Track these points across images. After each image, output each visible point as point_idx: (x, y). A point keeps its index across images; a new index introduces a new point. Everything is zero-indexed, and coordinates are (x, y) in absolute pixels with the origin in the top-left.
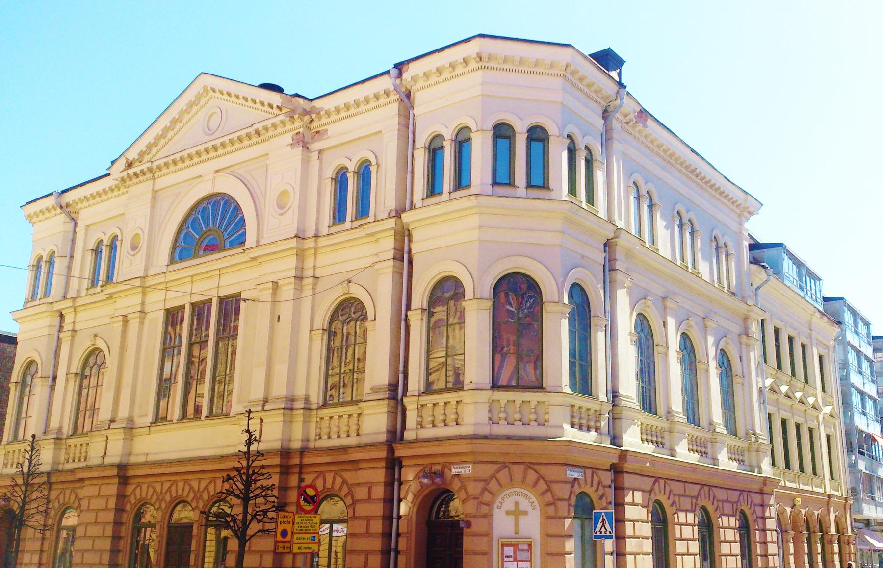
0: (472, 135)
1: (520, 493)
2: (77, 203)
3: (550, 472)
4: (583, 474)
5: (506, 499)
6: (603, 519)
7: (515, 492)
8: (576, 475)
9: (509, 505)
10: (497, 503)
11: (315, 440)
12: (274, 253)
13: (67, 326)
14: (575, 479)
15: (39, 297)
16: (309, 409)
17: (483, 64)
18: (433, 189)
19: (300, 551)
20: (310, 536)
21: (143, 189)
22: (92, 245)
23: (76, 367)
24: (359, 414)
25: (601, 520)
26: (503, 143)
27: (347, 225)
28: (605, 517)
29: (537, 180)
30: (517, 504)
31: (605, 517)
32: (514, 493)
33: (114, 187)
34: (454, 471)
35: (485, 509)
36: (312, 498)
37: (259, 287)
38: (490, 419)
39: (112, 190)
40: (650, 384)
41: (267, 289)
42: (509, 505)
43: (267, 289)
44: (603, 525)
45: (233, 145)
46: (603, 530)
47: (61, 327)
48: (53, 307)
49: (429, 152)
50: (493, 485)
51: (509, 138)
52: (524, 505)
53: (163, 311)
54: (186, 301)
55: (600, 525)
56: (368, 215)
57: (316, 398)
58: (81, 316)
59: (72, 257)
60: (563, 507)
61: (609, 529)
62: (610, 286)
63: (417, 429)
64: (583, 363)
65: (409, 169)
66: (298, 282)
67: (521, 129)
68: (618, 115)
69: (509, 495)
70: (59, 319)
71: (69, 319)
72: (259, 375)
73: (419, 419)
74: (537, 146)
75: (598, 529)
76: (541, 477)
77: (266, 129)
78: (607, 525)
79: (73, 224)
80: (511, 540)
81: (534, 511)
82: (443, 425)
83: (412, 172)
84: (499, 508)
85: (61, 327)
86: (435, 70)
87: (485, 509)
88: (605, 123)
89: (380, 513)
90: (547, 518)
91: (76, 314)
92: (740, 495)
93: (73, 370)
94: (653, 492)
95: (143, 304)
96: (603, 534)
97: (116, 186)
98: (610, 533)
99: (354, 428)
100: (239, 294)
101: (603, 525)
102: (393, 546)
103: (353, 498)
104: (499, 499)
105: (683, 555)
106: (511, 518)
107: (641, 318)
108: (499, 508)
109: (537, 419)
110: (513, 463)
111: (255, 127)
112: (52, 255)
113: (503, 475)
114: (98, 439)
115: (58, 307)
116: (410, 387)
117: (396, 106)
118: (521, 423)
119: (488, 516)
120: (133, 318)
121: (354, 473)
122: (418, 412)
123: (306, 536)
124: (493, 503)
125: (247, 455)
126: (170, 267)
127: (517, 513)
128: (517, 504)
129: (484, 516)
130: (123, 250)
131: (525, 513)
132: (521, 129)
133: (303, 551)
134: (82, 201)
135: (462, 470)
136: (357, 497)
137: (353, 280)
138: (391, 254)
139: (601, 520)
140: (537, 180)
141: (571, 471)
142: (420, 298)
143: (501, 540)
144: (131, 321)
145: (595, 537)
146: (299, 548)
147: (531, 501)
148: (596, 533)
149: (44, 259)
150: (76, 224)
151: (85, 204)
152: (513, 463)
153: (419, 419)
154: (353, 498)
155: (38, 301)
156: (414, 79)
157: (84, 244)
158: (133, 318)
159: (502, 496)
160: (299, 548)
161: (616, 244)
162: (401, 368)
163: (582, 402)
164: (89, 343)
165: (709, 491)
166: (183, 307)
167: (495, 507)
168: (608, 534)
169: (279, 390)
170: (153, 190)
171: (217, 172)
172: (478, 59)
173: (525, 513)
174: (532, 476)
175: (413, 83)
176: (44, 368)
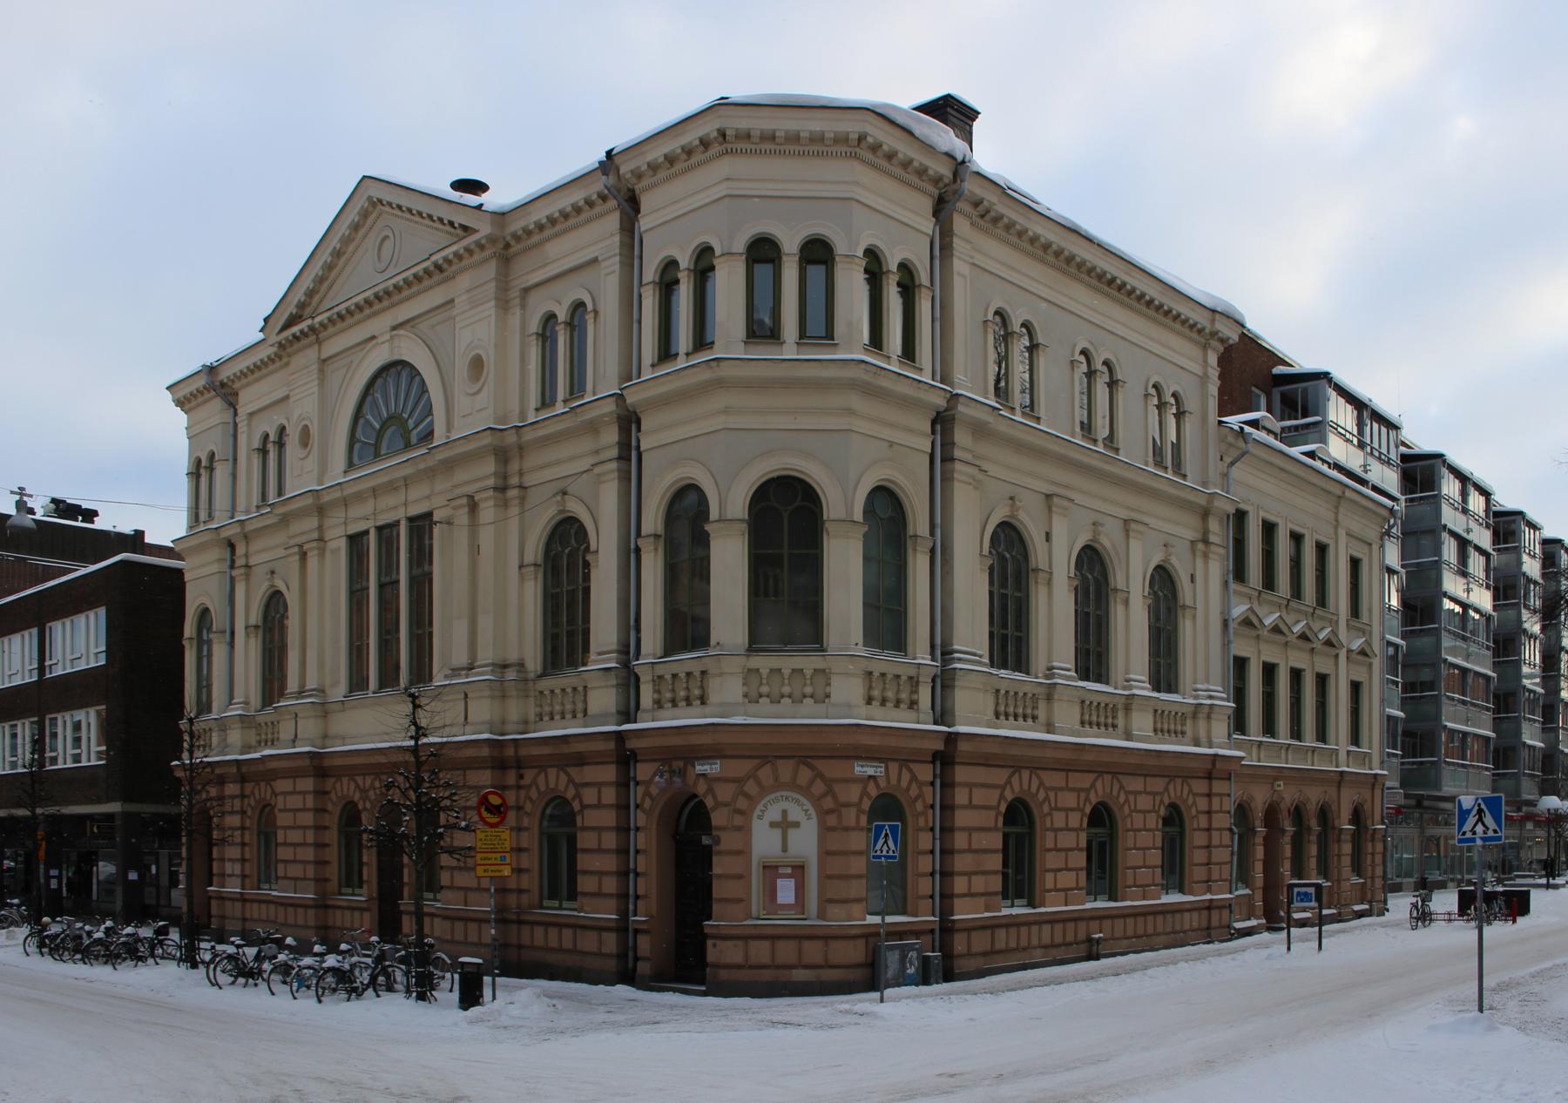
0: (716, 262)
2: (233, 381)
3: (832, 769)
4: (883, 769)
5: (769, 807)
6: (886, 835)
8: (870, 771)
9: (774, 813)
10: (757, 812)
11: (536, 722)
13: (240, 562)
14: (870, 777)
15: (561, 395)
16: (526, 680)
17: (729, 147)
18: (666, 353)
19: (486, 874)
20: (498, 855)
21: (307, 358)
22: (256, 444)
23: (255, 617)
24: (585, 687)
25: (883, 835)
26: (763, 271)
27: (560, 408)
28: (1483, 806)
29: (816, 325)
30: (785, 813)
31: (1483, 806)
33: (273, 356)
34: (699, 769)
35: (738, 820)
36: (497, 808)
37: (454, 504)
38: (745, 696)
39: (273, 361)
41: (461, 506)
43: (461, 506)
44: (886, 842)
45: (400, 292)
46: (1479, 829)
47: (233, 561)
48: (219, 534)
49: (660, 290)
50: (751, 787)
51: (771, 261)
52: (795, 813)
53: (344, 538)
54: (400, 514)
55: (881, 841)
56: (583, 389)
57: (534, 663)
58: (256, 545)
59: (235, 460)
60: (850, 817)
61: (892, 847)
63: (653, 709)
65: (635, 317)
66: (499, 495)
67: (790, 245)
68: (961, 205)
69: (776, 800)
70: (229, 549)
71: (240, 550)
72: (460, 630)
73: (656, 696)
74: (816, 273)
75: (1467, 827)
76: (820, 776)
77: (448, 261)
78: (891, 842)
79: (232, 410)
82: (699, 702)
83: (640, 322)
84: (760, 817)
85: (233, 561)
86: (697, 142)
87: (738, 820)
89: (613, 824)
90: (825, 830)
91: (247, 543)
93: (529, 558)
95: (320, 528)
96: (884, 853)
97: (276, 354)
98: (1495, 831)
99: (580, 706)
100: (429, 515)
101: (886, 842)
102: (632, 866)
103: (581, 802)
104: (760, 807)
106: (777, 833)
108: (760, 817)
110: (777, 757)
111: (434, 258)
112: (212, 455)
113: (765, 773)
114: (287, 717)
115: (225, 534)
116: (644, 650)
117: (616, 216)
118: (790, 701)
119: (745, 830)
120: (311, 549)
121: (578, 769)
122: (654, 685)
123: (494, 855)
124: (752, 811)
125: (415, 750)
126: (541, 412)
127: (785, 825)
128: (785, 813)
129: (739, 829)
130: (292, 449)
131: (797, 825)
132: (790, 245)
133: (490, 874)
134: (239, 378)
135: (707, 767)
136: (586, 802)
137: (569, 490)
138: (614, 452)
139: (883, 835)
140: (816, 325)
141: (862, 766)
142: (653, 520)
144: (482, 505)
145: (874, 857)
146: (485, 871)
147: (805, 808)
148: (1464, 833)
149: (272, 438)
150: (236, 414)
151: (244, 381)
152: (777, 757)
153: (656, 696)
154: (581, 802)
155: (682, 357)
157: (248, 441)
158: (311, 549)
159: (763, 802)
160: (485, 871)
161: (954, 419)
162: (632, 622)
163: (887, 662)
164: (266, 585)
167: (755, 816)
168: (891, 853)
169: (486, 655)
170: (319, 358)
171: (394, 328)
172: (721, 139)
173: (797, 825)
174: (805, 774)
176: (219, 619)
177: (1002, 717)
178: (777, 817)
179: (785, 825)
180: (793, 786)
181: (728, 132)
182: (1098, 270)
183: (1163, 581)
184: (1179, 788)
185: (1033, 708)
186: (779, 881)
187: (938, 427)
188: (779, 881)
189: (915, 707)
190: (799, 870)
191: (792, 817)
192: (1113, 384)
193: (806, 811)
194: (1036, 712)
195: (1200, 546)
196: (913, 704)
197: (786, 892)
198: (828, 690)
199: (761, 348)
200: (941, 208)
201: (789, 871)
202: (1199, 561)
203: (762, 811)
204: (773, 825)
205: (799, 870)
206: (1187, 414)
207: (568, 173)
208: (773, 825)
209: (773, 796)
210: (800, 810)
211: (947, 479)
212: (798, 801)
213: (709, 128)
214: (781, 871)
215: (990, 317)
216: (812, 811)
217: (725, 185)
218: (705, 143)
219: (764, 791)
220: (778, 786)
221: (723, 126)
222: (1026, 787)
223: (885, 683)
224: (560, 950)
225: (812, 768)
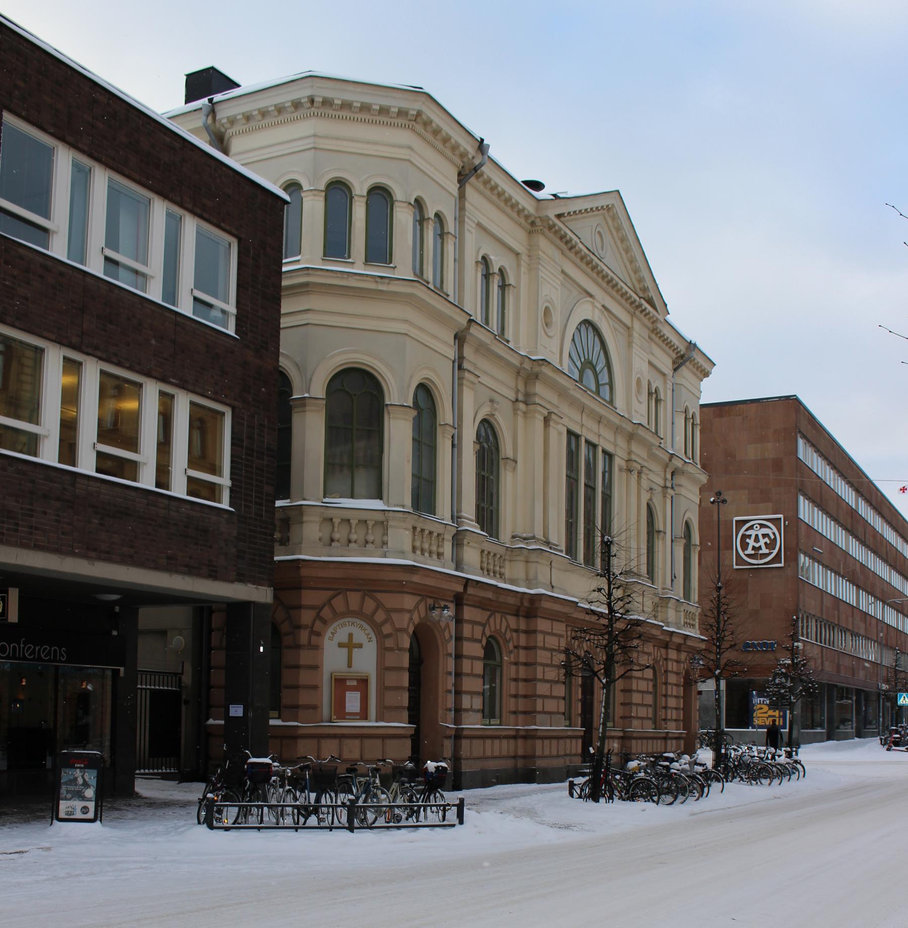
1: (355, 624)
5: (338, 630)
7: (349, 622)
9: (342, 635)
12: (368, 143)
30: (351, 636)
32: (347, 623)
40: (492, 504)
42: (342, 635)
62: (458, 384)
64: (485, 474)
67: (360, 189)
80: (345, 674)
81: (370, 643)
84: (331, 639)
88: (460, 187)
92: (420, 602)
94: (487, 626)
104: (331, 630)
105: (558, 713)
107: (486, 425)
109: (374, 541)
119: (317, 648)
127: (350, 645)
128: (351, 636)
131: (360, 646)
132: (360, 189)
143: (334, 674)
147: (367, 632)
156: (232, 121)
165: (501, 619)
166: (145, 263)
167: (326, 637)
173: (360, 646)
175: (228, 125)
177: (418, 552)
178: (345, 640)
179: (350, 645)
180: (359, 614)
181: (316, 99)
182: (513, 201)
183: (487, 428)
184: (498, 621)
185: (438, 546)
186: (347, 693)
187: (457, 341)
188: (347, 693)
189: (503, 577)
190: (363, 682)
191: (345, 640)
192: (503, 287)
193: (368, 634)
194: (502, 570)
195: (522, 406)
196: (440, 555)
197: (353, 702)
198: (385, 538)
199: (335, 266)
200: (463, 178)
201: (355, 683)
202: (520, 420)
203: (333, 634)
204: (341, 645)
205: (363, 682)
206: (511, 287)
207: (613, 361)
208: (341, 645)
209: (341, 621)
210: (362, 633)
211: (461, 385)
212: (361, 627)
213: (301, 93)
214: (348, 683)
215: (480, 259)
216: (373, 635)
217: (311, 140)
218: (297, 105)
219: (337, 615)
220: (349, 613)
221: (313, 94)
222: (498, 628)
223: (431, 540)
224: (551, 757)
225: (375, 599)
